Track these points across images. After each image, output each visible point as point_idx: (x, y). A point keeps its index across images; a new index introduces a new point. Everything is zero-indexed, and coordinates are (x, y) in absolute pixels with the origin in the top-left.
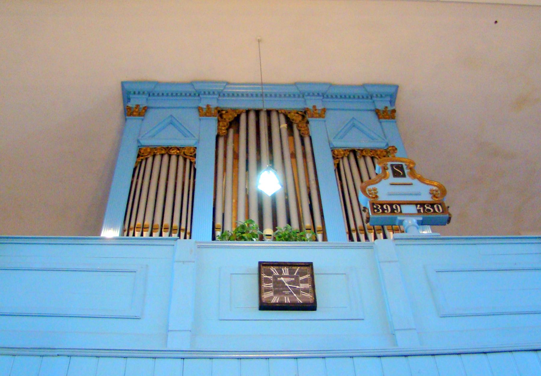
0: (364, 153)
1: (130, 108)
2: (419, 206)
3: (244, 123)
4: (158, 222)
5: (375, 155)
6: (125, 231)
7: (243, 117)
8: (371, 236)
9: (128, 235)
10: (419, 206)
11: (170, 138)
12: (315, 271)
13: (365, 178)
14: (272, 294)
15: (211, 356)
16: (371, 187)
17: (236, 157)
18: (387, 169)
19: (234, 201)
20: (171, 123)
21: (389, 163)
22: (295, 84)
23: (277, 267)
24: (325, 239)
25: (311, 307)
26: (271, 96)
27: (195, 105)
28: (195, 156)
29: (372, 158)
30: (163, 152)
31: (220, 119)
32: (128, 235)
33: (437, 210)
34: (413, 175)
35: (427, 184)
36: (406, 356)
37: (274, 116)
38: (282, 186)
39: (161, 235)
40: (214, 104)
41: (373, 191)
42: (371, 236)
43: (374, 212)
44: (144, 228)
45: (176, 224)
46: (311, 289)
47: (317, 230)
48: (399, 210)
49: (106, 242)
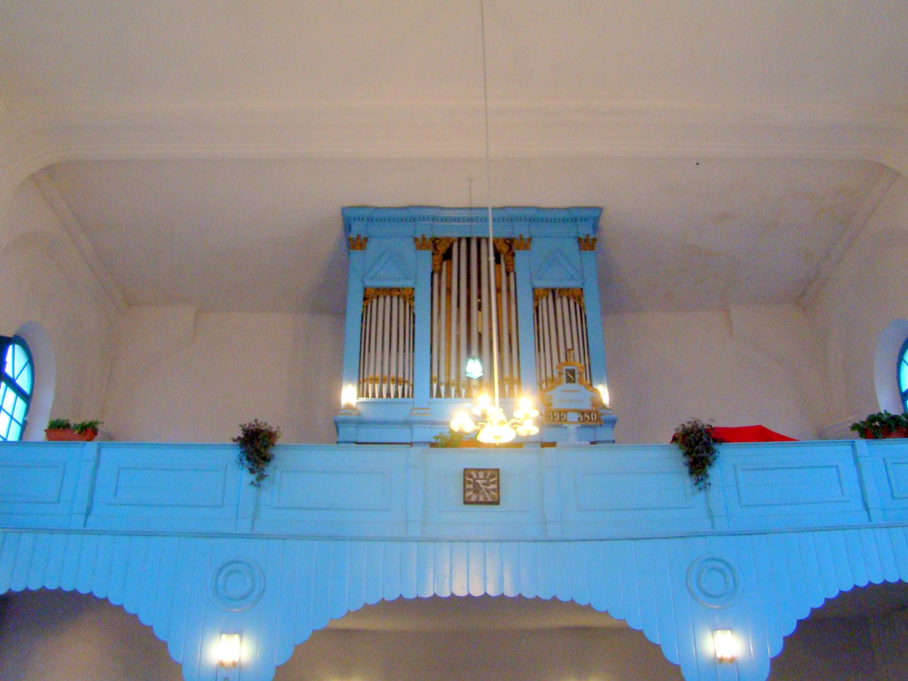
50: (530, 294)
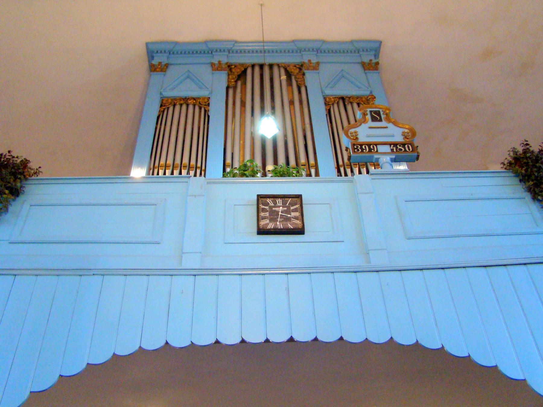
0: (351, 100)
1: (154, 65)
2: (392, 146)
3: (252, 76)
4: (178, 161)
5: (363, 101)
6: (150, 169)
7: (249, 71)
8: (356, 170)
9: (153, 174)
10: (392, 146)
11: (189, 90)
12: (304, 202)
13: (352, 121)
14: (268, 221)
15: (216, 273)
16: (352, 130)
17: (243, 104)
18: (367, 115)
19: (241, 142)
20: (188, 77)
21: (369, 110)
22: (293, 41)
23: (273, 199)
24: (317, 174)
25: (300, 231)
26: (273, 52)
27: (209, 62)
28: (209, 105)
29: (358, 104)
30: (182, 102)
31: (230, 73)
32: (153, 174)
33: (407, 149)
34: (388, 120)
35: (400, 127)
36: (377, 271)
37: (276, 69)
38: (279, 130)
39: (180, 173)
40: (224, 60)
41: (354, 134)
42: (356, 170)
43: (355, 152)
44: (166, 166)
45: (193, 162)
46: (300, 217)
47: (310, 165)
48: (376, 150)
49: (134, 182)
50: (322, 101)
